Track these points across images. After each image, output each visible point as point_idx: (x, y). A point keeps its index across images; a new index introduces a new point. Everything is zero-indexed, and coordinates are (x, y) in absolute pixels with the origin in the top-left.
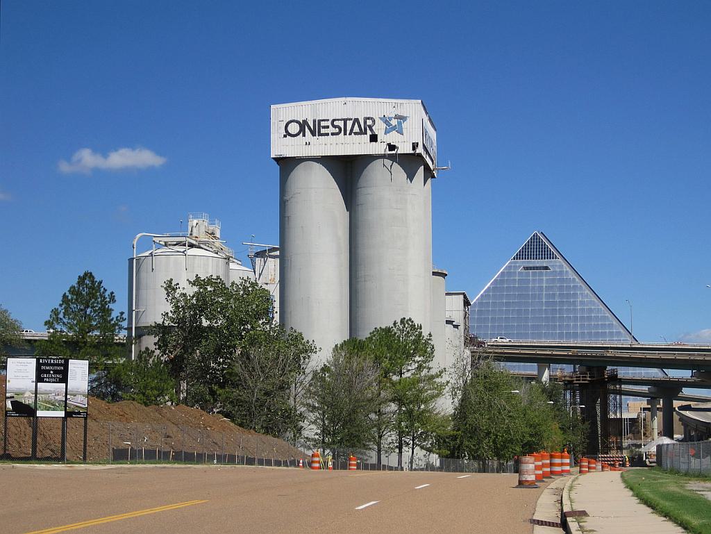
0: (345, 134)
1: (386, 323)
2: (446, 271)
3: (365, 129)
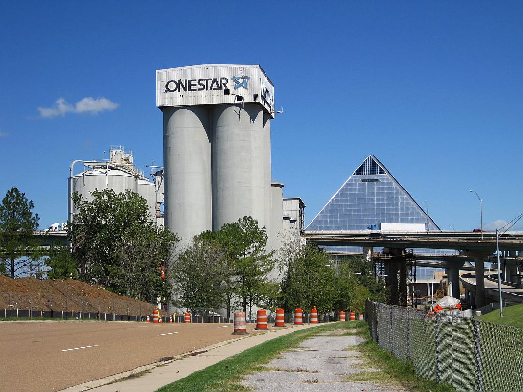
0: (207, 89)
1: (233, 219)
2: (283, 183)
3: (221, 86)
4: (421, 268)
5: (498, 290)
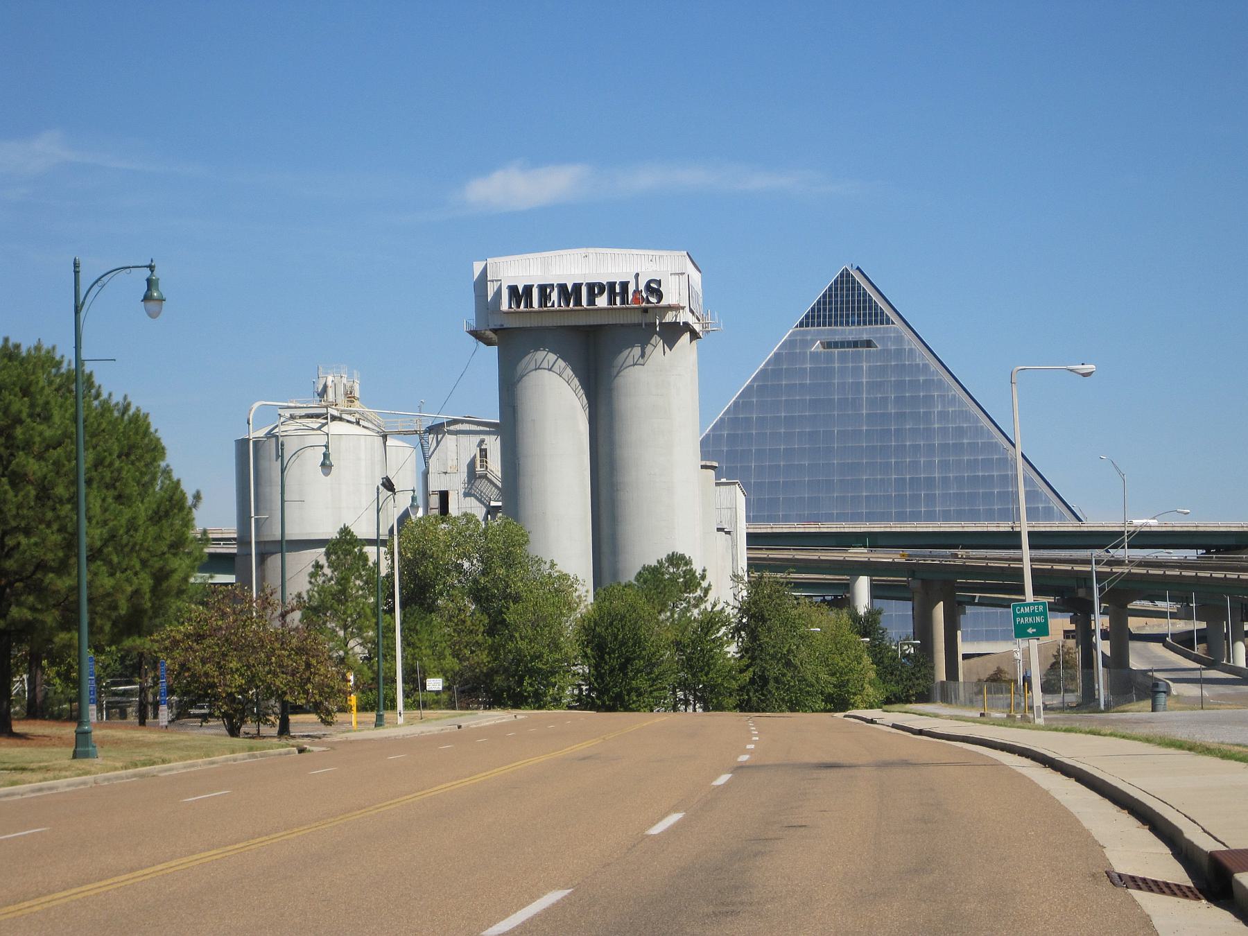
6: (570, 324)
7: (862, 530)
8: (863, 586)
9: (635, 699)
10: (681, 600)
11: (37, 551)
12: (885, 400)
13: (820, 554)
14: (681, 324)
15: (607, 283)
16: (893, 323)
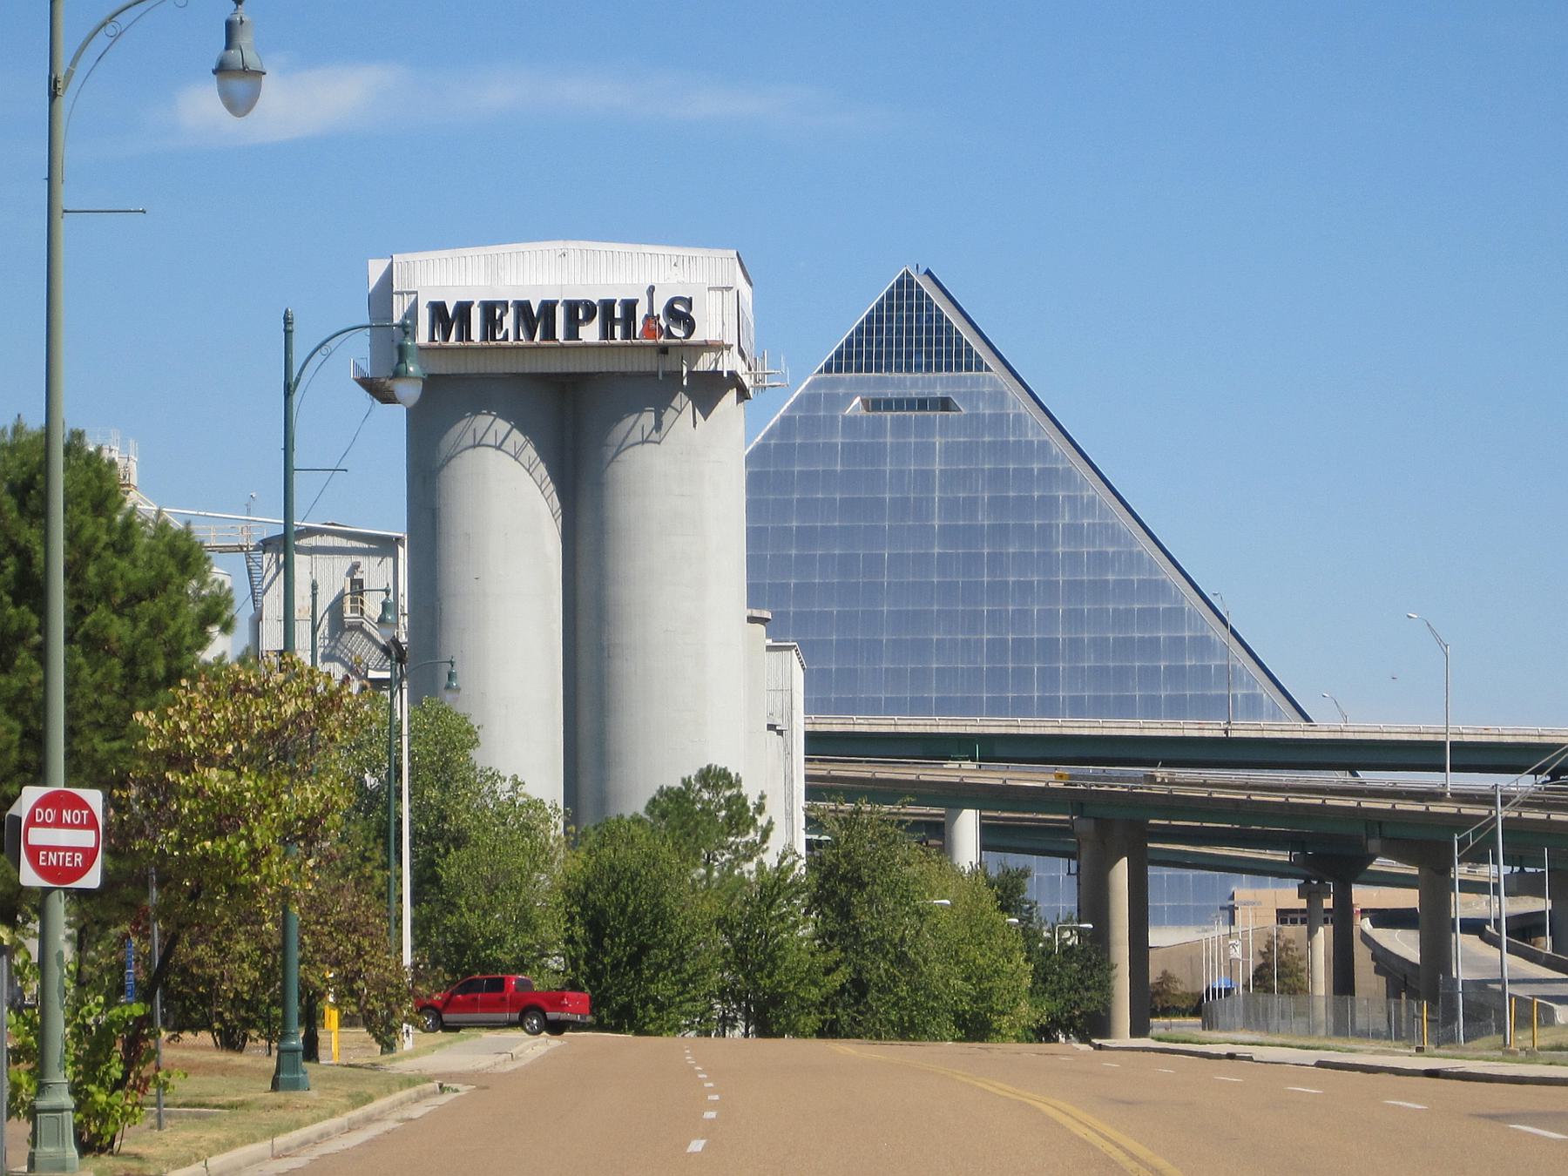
4: (1167, 872)
5: (1498, 987)
6: (534, 371)
7: (969, 730)
8: (968, 825)
9: (654, 1014)
10: (723, 848)
11: (127, 763)
12: (972, 503)
13: (919, 772)
14: (725, 375)
15: (600, 301)
16: (988, 369)
